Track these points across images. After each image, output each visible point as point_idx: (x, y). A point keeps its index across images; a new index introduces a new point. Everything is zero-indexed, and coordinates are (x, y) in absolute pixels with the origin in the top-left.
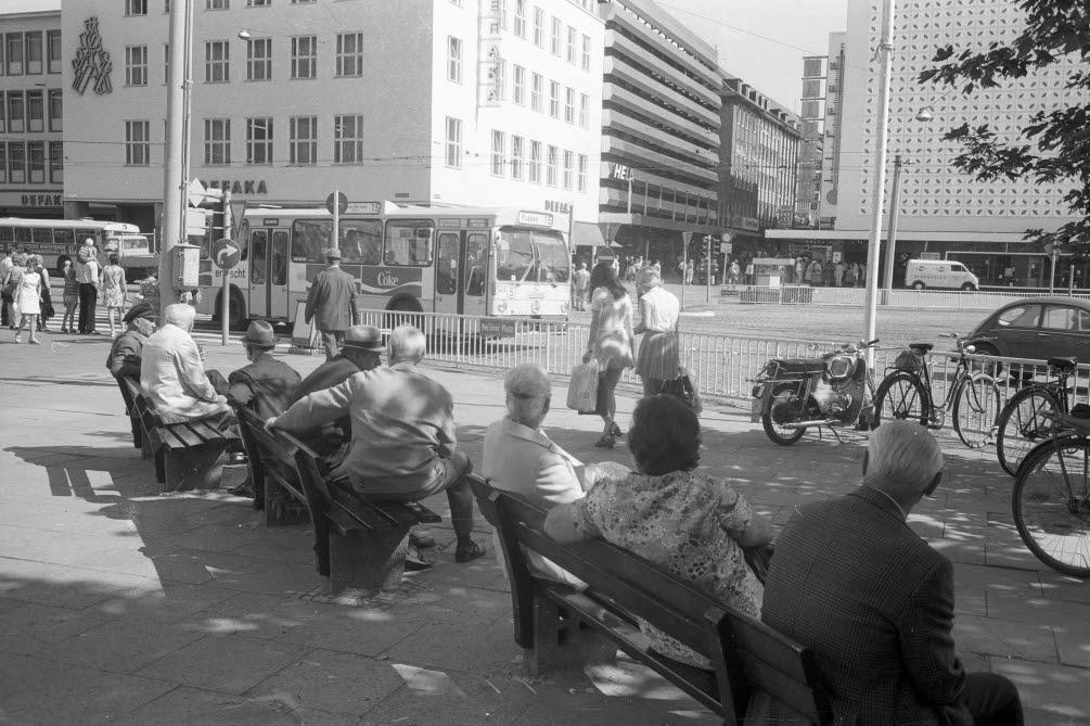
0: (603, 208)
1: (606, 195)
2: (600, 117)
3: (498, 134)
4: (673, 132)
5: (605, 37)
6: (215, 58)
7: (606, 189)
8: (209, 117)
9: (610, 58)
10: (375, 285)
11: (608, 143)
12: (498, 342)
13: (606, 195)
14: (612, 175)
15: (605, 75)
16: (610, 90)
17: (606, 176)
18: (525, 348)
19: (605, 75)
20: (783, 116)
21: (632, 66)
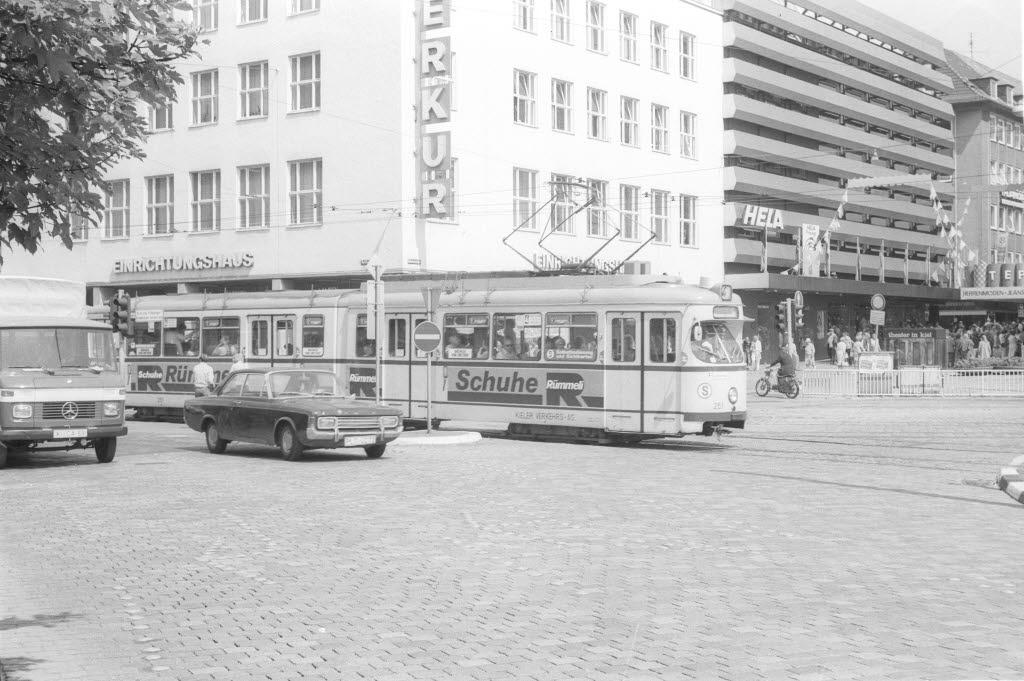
0: (731, 267)
1: (731, 250)
2: (717, 69)
3: (524, 78)
4: (849, 89)
5: (718, 34)
6: (209, 100)
7: (732, 95)
8: (195, 169)
9: (731, 60)
10: (209, 355)
11: (732, 177)
12: (969, 371)
13: (731, 250)
14: (740, 220)
15: (725, 84)
16: (732, 105)
17: (732, 223)
18: (869, 379)
19: (725, 84)
20: (1002, 89)
21: (758, 169)
